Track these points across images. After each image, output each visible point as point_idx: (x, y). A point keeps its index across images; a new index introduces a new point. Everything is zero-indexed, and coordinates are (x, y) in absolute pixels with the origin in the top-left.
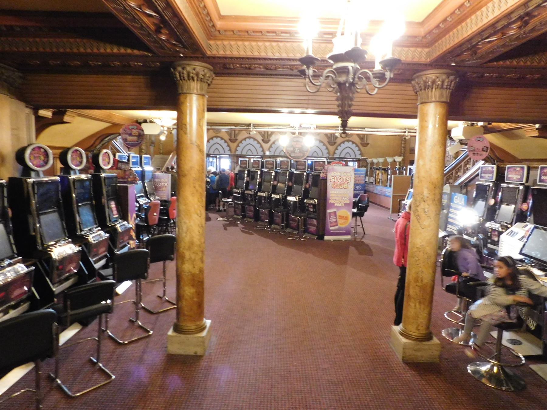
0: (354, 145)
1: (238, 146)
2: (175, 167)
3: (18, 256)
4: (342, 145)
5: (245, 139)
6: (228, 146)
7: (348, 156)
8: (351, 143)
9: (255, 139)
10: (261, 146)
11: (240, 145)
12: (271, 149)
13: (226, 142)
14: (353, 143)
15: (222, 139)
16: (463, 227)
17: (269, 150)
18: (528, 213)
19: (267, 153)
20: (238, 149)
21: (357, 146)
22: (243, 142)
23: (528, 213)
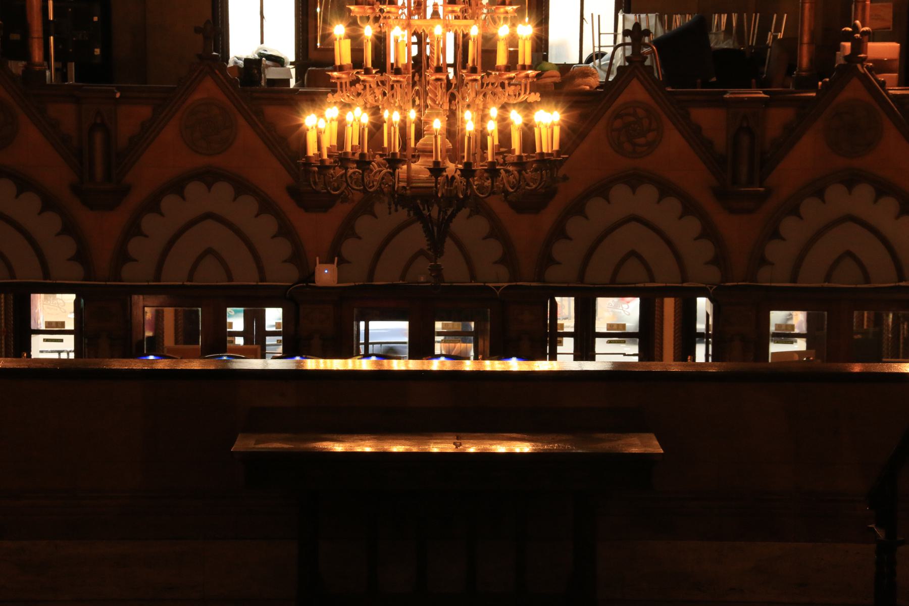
0: (673, 205)
1: (134, 229)
2: (441, 184)
3: (500, 169)
4: (169, 202)
5: (177, 187)
6: (69, 228)
7: (846, 279)
8: (648, 192)
9: (242, 187)
10: (286, 230)
11: (149, 222)
12: (349, 247)
13: (49, 204)
14: (666, 189)
15: (242, 187)
16: (320, 105)
17: (333, 255)
18: (384, 157)
19: (326, 274)
20: (134, 246)
21: (690, 207)
22: (169, 202)
23: (384, 157)
